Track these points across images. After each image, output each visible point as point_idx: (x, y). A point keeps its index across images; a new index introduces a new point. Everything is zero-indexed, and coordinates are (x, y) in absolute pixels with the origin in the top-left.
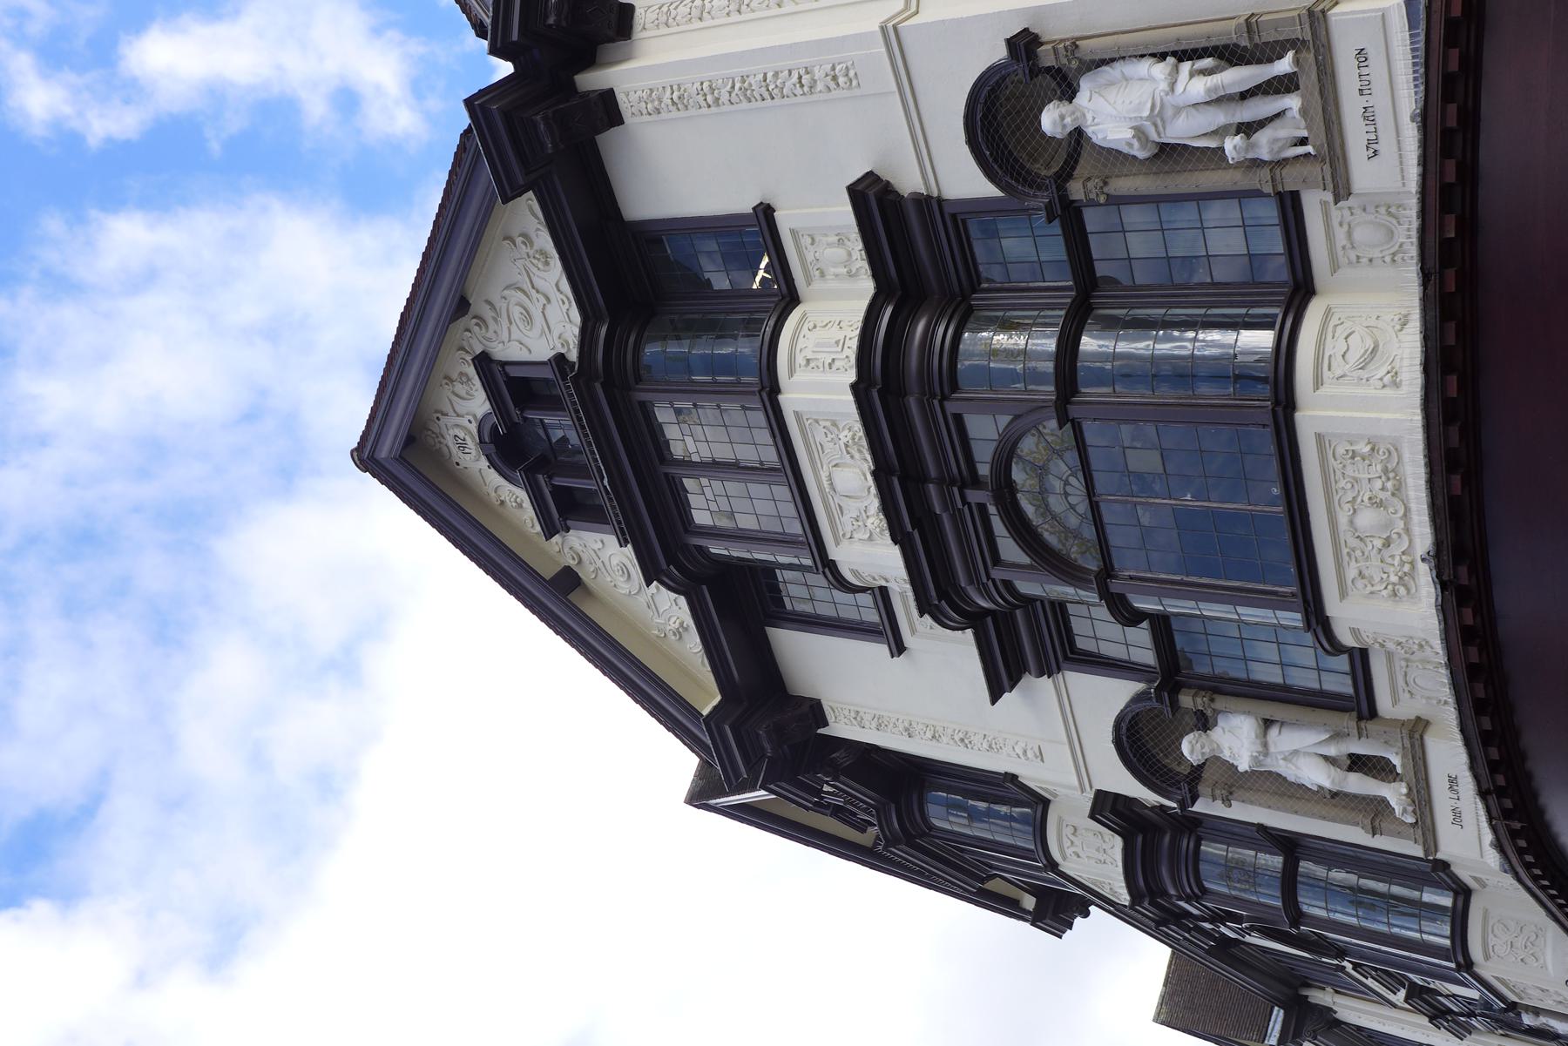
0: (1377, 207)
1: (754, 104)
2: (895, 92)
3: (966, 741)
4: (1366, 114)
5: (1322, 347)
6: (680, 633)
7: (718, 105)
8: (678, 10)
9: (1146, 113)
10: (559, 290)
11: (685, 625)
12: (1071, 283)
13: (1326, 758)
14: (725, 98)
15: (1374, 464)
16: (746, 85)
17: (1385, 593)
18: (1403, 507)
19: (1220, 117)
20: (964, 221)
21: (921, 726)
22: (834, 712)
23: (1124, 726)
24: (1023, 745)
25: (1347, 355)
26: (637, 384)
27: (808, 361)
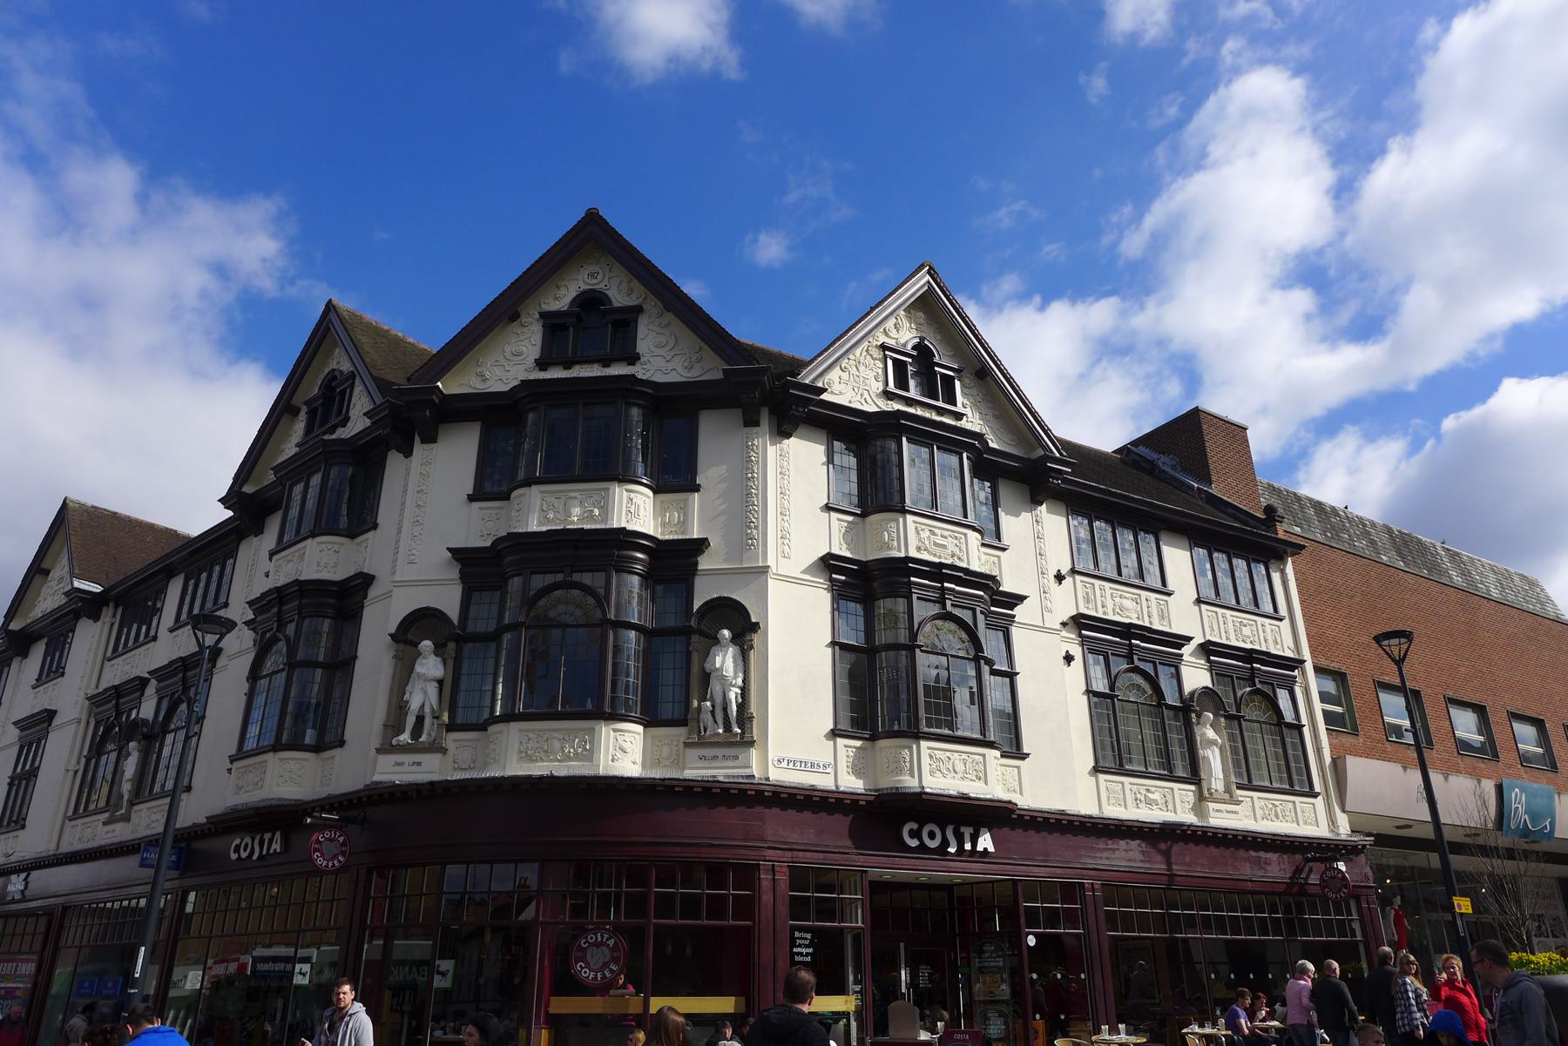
1: (745, 497)
13: (423, 705)
19: (719, 700)
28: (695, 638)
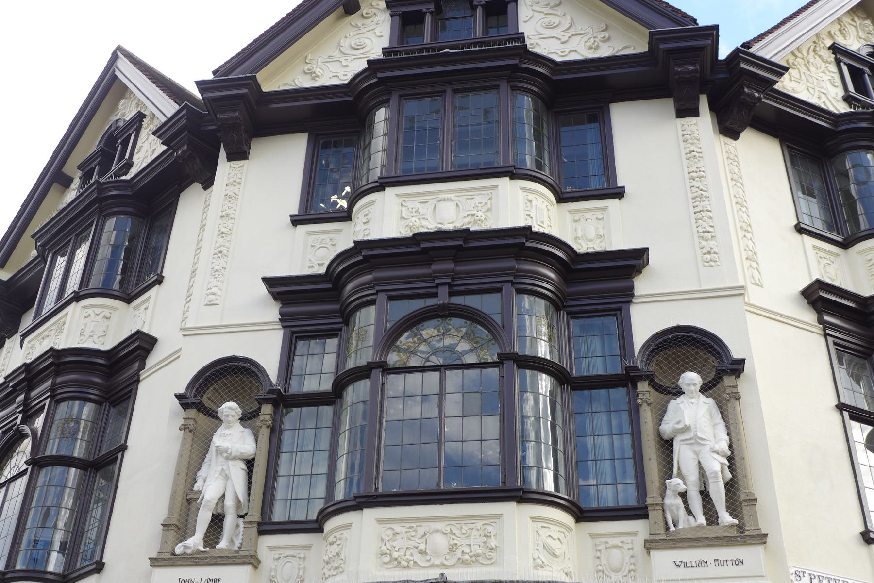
0: (634, 564)
1: (691, 201)
2: (701, 287)
3: (220, 255)
4: (702, 562)
5: (554, 523)
6: (310, 73)
7: (690, 179)
8: (736, 167)
9: (699, 435)
10: (571, 51)
11: (317, 78)
12: (575, 375)
14: (694, 183)
15: (481, 548)
16: (704, 198)
17: (384, 548)
18: (451, 564)
20: (615, 315)
21: (230, 225)
22: (239, 167)
23: (247, 365)
24: (219, 294)
25: (550, 538)
26: (511, 87)
27: (531, 201)
28: (643, 387)
